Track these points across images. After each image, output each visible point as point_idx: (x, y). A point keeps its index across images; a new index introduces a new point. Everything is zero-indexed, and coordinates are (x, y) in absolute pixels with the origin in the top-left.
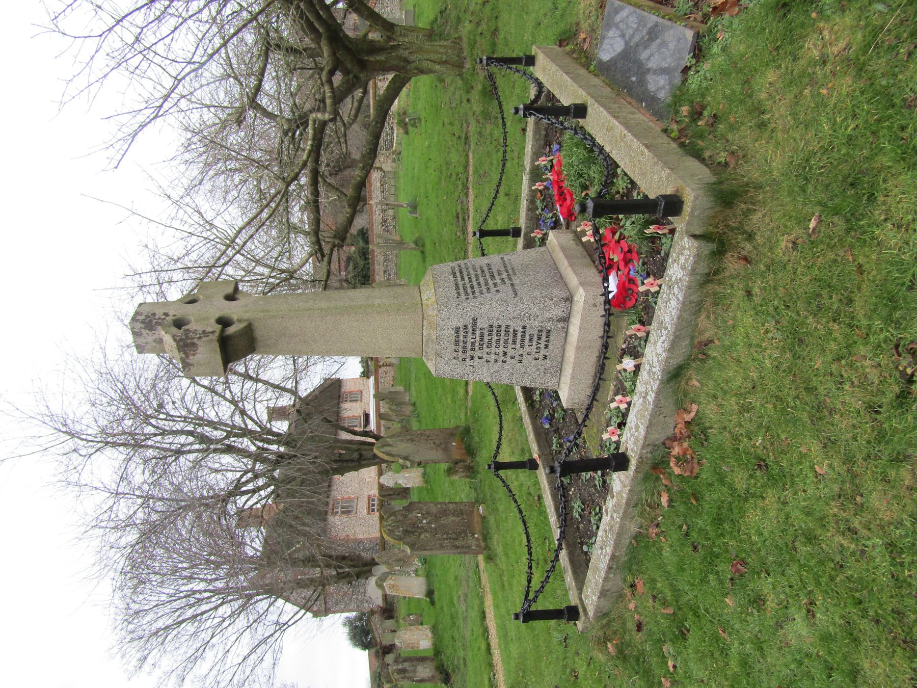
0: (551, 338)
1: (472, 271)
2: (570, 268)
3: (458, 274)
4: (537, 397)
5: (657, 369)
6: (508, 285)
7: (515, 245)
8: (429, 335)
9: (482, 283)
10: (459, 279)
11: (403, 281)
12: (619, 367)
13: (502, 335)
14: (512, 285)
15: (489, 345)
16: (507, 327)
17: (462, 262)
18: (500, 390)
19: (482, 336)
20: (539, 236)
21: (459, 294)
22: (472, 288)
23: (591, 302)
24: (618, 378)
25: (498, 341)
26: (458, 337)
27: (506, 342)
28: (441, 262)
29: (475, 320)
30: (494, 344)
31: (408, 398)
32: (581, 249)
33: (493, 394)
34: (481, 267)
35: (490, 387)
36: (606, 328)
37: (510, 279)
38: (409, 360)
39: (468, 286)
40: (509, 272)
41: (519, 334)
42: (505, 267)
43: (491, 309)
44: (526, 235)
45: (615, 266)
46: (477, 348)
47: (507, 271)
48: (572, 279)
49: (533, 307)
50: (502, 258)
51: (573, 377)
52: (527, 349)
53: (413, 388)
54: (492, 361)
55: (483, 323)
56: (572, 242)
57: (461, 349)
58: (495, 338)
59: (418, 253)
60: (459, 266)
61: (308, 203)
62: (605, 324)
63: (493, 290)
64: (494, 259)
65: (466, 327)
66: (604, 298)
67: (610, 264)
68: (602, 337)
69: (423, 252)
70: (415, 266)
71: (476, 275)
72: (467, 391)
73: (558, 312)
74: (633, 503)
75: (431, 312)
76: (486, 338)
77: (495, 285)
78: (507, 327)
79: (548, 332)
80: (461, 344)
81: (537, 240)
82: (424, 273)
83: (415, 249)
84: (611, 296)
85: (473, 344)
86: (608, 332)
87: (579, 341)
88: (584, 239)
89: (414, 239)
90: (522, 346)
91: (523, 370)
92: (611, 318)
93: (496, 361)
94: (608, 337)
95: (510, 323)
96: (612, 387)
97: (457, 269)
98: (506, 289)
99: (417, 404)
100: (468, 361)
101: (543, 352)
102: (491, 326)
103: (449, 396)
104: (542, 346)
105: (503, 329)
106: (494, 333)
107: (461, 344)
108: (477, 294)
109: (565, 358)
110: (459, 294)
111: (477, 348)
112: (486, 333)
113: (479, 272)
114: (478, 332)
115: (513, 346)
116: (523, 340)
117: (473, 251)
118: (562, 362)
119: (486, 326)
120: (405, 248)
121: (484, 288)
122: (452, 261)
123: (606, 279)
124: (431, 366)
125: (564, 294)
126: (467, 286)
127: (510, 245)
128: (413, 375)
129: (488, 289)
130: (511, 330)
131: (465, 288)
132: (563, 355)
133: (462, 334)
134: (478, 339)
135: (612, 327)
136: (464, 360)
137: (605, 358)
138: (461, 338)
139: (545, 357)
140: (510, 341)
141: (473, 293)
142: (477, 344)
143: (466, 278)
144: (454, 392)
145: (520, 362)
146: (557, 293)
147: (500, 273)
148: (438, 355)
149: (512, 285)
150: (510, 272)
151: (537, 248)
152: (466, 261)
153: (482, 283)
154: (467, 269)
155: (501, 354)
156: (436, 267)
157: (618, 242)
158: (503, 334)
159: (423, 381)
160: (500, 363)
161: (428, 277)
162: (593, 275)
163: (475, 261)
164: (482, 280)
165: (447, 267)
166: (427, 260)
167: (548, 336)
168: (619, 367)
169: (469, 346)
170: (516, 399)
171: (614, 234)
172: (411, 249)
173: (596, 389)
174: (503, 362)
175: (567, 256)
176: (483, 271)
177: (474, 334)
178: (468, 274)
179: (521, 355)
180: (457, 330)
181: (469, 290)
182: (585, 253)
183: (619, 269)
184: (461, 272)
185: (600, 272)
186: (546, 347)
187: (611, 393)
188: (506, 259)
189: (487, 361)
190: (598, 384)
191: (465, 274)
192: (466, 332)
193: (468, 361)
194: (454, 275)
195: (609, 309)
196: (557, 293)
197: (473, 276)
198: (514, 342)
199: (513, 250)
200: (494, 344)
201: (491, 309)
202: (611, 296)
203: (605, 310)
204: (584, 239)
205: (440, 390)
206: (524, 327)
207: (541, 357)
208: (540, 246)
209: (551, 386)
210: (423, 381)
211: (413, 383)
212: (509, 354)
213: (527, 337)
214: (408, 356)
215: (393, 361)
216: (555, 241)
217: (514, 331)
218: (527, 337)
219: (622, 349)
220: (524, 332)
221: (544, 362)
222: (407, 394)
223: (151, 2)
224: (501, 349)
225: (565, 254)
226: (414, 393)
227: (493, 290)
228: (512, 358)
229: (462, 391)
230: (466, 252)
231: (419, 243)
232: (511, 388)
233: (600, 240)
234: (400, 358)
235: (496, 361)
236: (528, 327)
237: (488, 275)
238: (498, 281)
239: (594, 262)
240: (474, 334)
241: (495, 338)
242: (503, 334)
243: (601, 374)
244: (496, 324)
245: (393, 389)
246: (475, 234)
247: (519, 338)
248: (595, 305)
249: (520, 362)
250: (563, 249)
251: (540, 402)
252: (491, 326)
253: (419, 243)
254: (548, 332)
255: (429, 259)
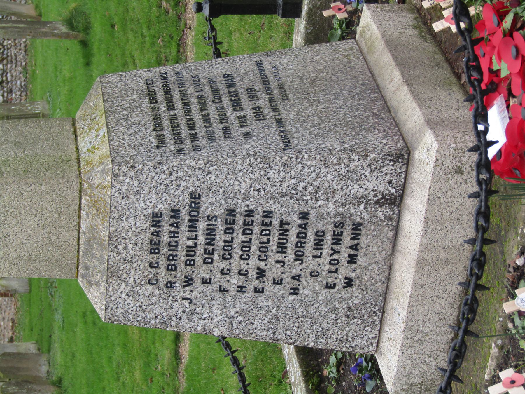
0: (364, 241)
2: (405, 89)
3: (160, 96)
4: (330, 371)
7: (289, 34)
8: (93, 228)
9: (214, 116)
10: (163, 107)
11: (39, 107)
12: (508, 307)
13: (254, 232)
14: (279, 122)
15: (226, 256)
16: (267, 214)
17: (169, 69)
18: (251, 354)
19: (210, 233)
20: (342, 16)
21: (161, 139)
23: (450, 163)
24: (506, 330)
25: (246, 245)
26: (156, 234)
27: (264, 247)
28: (125, 66)
29: (195, 198)
30: (237, 252)
31: (44, 368)
32: (430, 47)
33: (235, 361)
34: (211, 82)
35: (228, 346)
36: (482, 222)
37: (275, 109)
38: (50, 284)
39: (182, 122)
40: (272, 92)
41: (293, 232)
42: (265, 81)
43: (233, 175)
44: (310, 12)
45: (504, 86)
46: (199, 260)
47: (268, 91)
48: (411, 113)
49: (323, 171)
50: (259, 64)
51: (408, 328)
52: (310, 263)
53: (56, 346)
54: (233, 290)
55: (213, 206)
56: (412, 32)
57: (163, 263)
58: (239, 238)
59: (74, 46)
60: (164, 77)
61: (130, 332)
62: (479, 213)
63: (237, 132)
64: (242, 66)
65: (175, 213)
66: (475, 157)
67: (491, 82)
68: (472, 242)
69: (84, 44)
70: (66, 73)
71: (201, 100)
72: (177, 356)
73: (377, 184)
74: (97, 321)
75: (99, 178)
76: (220, 238)
77: (242, 121)
78: (267, 214)
79: (357, 227)
80: (164, 250)
81: (336, 25)
82: (87, 90)
83: (67, 36)
84: (492, 152)
85: (191, 250)
86: (485, 230)
87: (423, 249)
88: (438, 26)
89: (66, 14)
90: (299, 257)
91: (300, 312)
92: (493, 199)
93: (241, 289)
94: (486, 242)
95: (273, 206)
96: (494, 351)
97: (158, 84)
98: (265, 131)
99: (66, 383)
100: (179, 291)
101: (344, 271)
102: (231, 212)
103: (137, 365)
104: (343, 257)
105: (258, 218)
106: (238, 228)
107: (164, 250)
108: (201, 141)
109: (392, 286)
110: (161, 139)
111: (199, 260)
112: (221, 228)
113: (207, 92)
114: (202, 225)
115: (279, 257)
116: (300, 244)
117: (196, 44)
118: (386, 294)
119: (220, 211)
120: (45, 35)
121: (217, 128)
122: (149, 66)
123: (481, 116)
124: (96, 298)
125: (392, 145)
126: (179, 122)
127: (279, 34)
128: (58, 317)
130: (276, 222)
132: (388, 279)
133: (166, 228)
134: (202, 239)
135: (494, 219)
136: (170, 285)
137: (479, 287)
138: (165, 238)
139: (349, 282)
140: (273, 246)
141: (194, 137)
142: (200, 250)
143: (179, 104)
144: (149, 357)
145: (295, 291)
146: (378, 141)
147: (252, 95)
148: (112, 274)
149: (279, 122)
150: (276, 92)
151: (336, 43)
152: (178, 67)
153: (214, 116)
154: (181, 84)
155: (253, 274)
156: (113, 78)
157: (509, 34)
158: (256, 229)
159: (79, 330)
160: (249, 294)
161: (95, 100)
162: (455, 104)
163: (201, 67)
164: (212, 109)
165: (136, 79)
166: (95, 60)
167: (355, 237)
168: (508, 307)
169: (181, 255)
170: (285, 374)
171: (501, 17)
172: (61, 36)
173: (459, 354)
174: (257, 291)
175: (400, 63)
176: (215, 91)
177: (192, 228)
178: (183, 95)
179: (297, 278)
180: (156, 219)
181: (185, 132)
182: (439, 57)
183: (510, 94)
184: (167, 91)
185: (470, 99)
186: (352, 259)
187: (491, 363)
188: (266, 65)
189: (222, 290)
190: (463, 343)
191: (176, 97)
192: (176, 225)
193: (179, 291)
194: (152, 97)
195: (488, 182)
196: (378, 141)
197: (193, 100)
198: (282, 248)
199: (284, 46)
200: (237, 252)
201: (233, 175)
202: (492, 152)
203: (480, 183)
204: (438, 26)
205: (119, 350)
206: (304, 216)
207: (341, 281)
208: (342, 38)
209: (361, 345)
210: (79, 330)
211: (57, 335)
212: (270, 275)
213: (311, 236)
214: (45, 275)
215: (14, 285)
216: (374, 28)
217: (282, 223)
218: (311, 236)
219: (517, 268)
220: (304, 227)
221: (345, 294)
222: (43, 360)
224: (253, 263)
225: (395, 58)
226: (59, 358)
227: (237, 132)
228: (275, 282)
229: (166, 355)
230: (181, 44)
231: (78, 25)
232: (272, 349)
233: (470, 30)
234: (30, 281)
235: (241, 289)
236: (313, 215)
237: (226, 100)
238: (249, 113)
239: (459, 77)
240: (192, 228)
241: (239, 238)
242: (256, 229)
243: (469, 322)
244: (242, 208)
245: (11, 349)
246: (199, 8)
247: (293, 238)
248: (459, 171)
249: (295, 291)
250: (392, 45)
251: (338, 381)
252: (231, 212)
253: (78, 25)
254: (357, 227)
255: (99, 59)
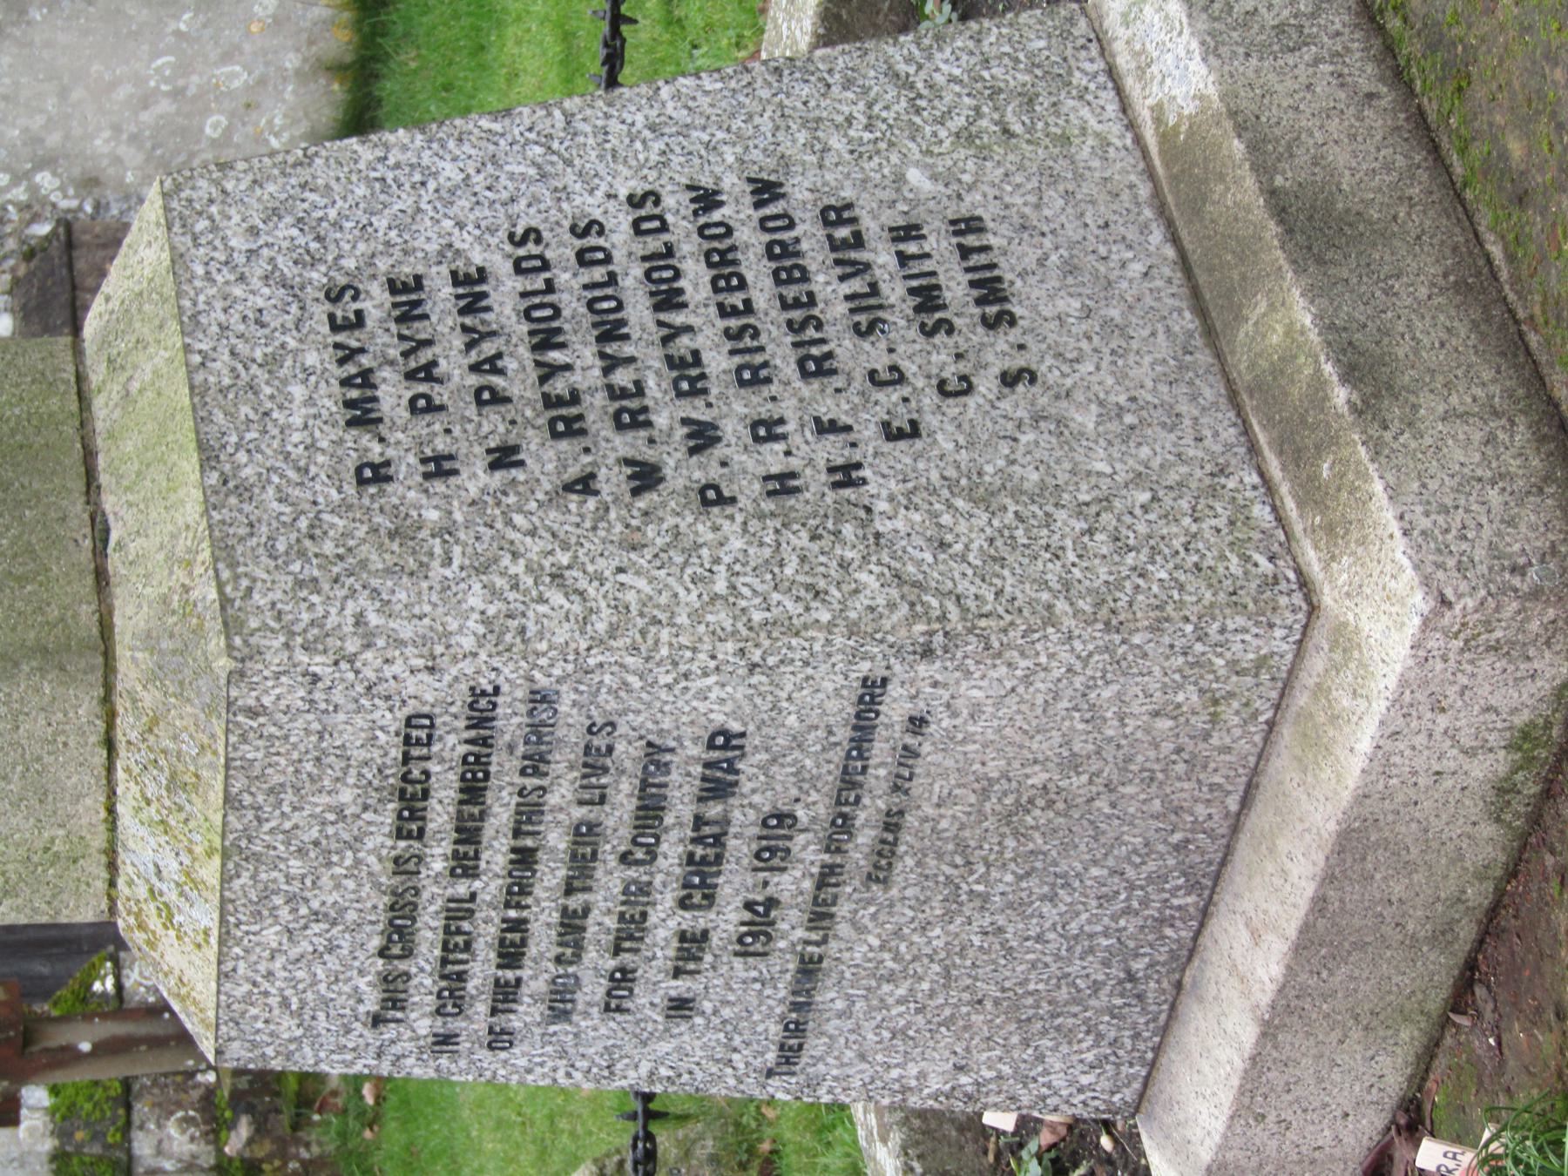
1: (562, 792)
3: (441, 812)
5: (1230, 991)
6: (782, 964)
9: (602, 922)
21: (394, 997)
22: (511, 955)
108: (527, 1013)
110: (394, 997)
129: (622, 979)
131: (455, 945)
141: (505, 995)
181: (482, 969)
194: (411, 803)
223: (1562, 426)
236: (941, 723)
238: (727, 919)
